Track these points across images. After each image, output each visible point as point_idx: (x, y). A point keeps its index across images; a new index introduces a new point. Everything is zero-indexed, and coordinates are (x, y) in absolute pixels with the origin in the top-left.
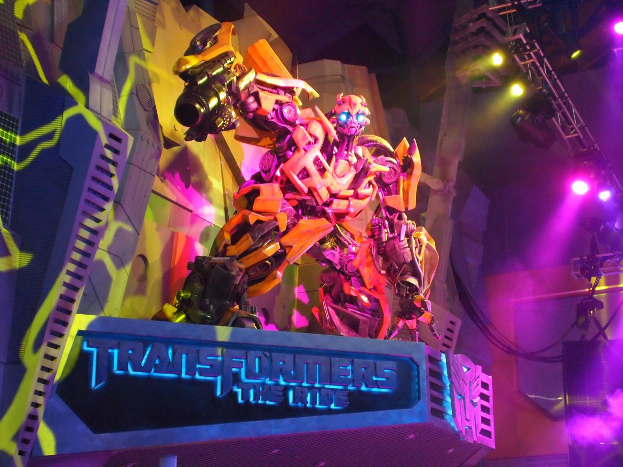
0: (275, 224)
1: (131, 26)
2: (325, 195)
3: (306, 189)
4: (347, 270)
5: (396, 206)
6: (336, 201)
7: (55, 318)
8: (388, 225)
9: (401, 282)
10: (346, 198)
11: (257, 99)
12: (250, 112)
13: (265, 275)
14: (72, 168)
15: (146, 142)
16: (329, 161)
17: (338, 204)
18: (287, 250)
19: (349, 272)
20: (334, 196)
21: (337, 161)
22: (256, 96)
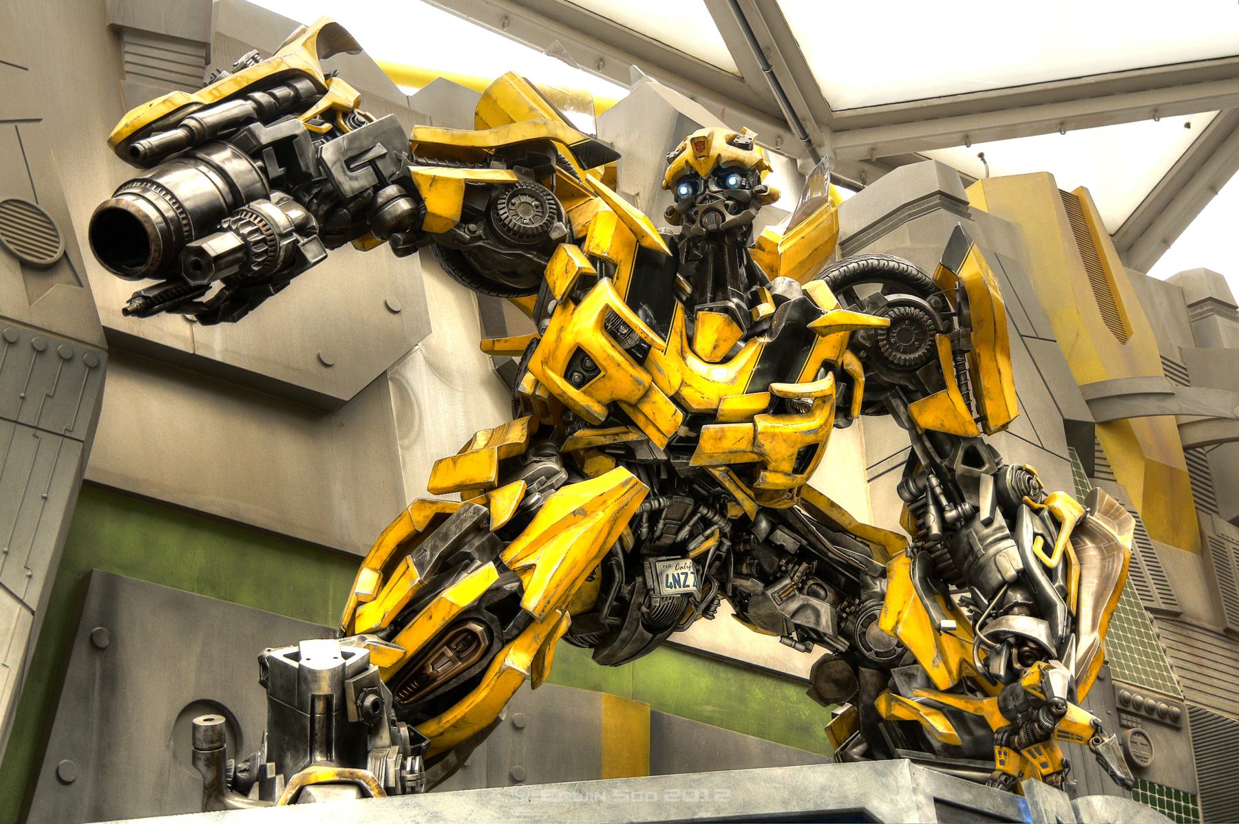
1: (1021, 336)
3: (598, 410)
4: (870, 650)
5: (952, 426)
11: (410, 189)
13: (476, 671)
14: (25, 567)
16: (661, 324)
17: (720, 438)
19: (877, 653)
20: (698, 419)
21: (691, 319)
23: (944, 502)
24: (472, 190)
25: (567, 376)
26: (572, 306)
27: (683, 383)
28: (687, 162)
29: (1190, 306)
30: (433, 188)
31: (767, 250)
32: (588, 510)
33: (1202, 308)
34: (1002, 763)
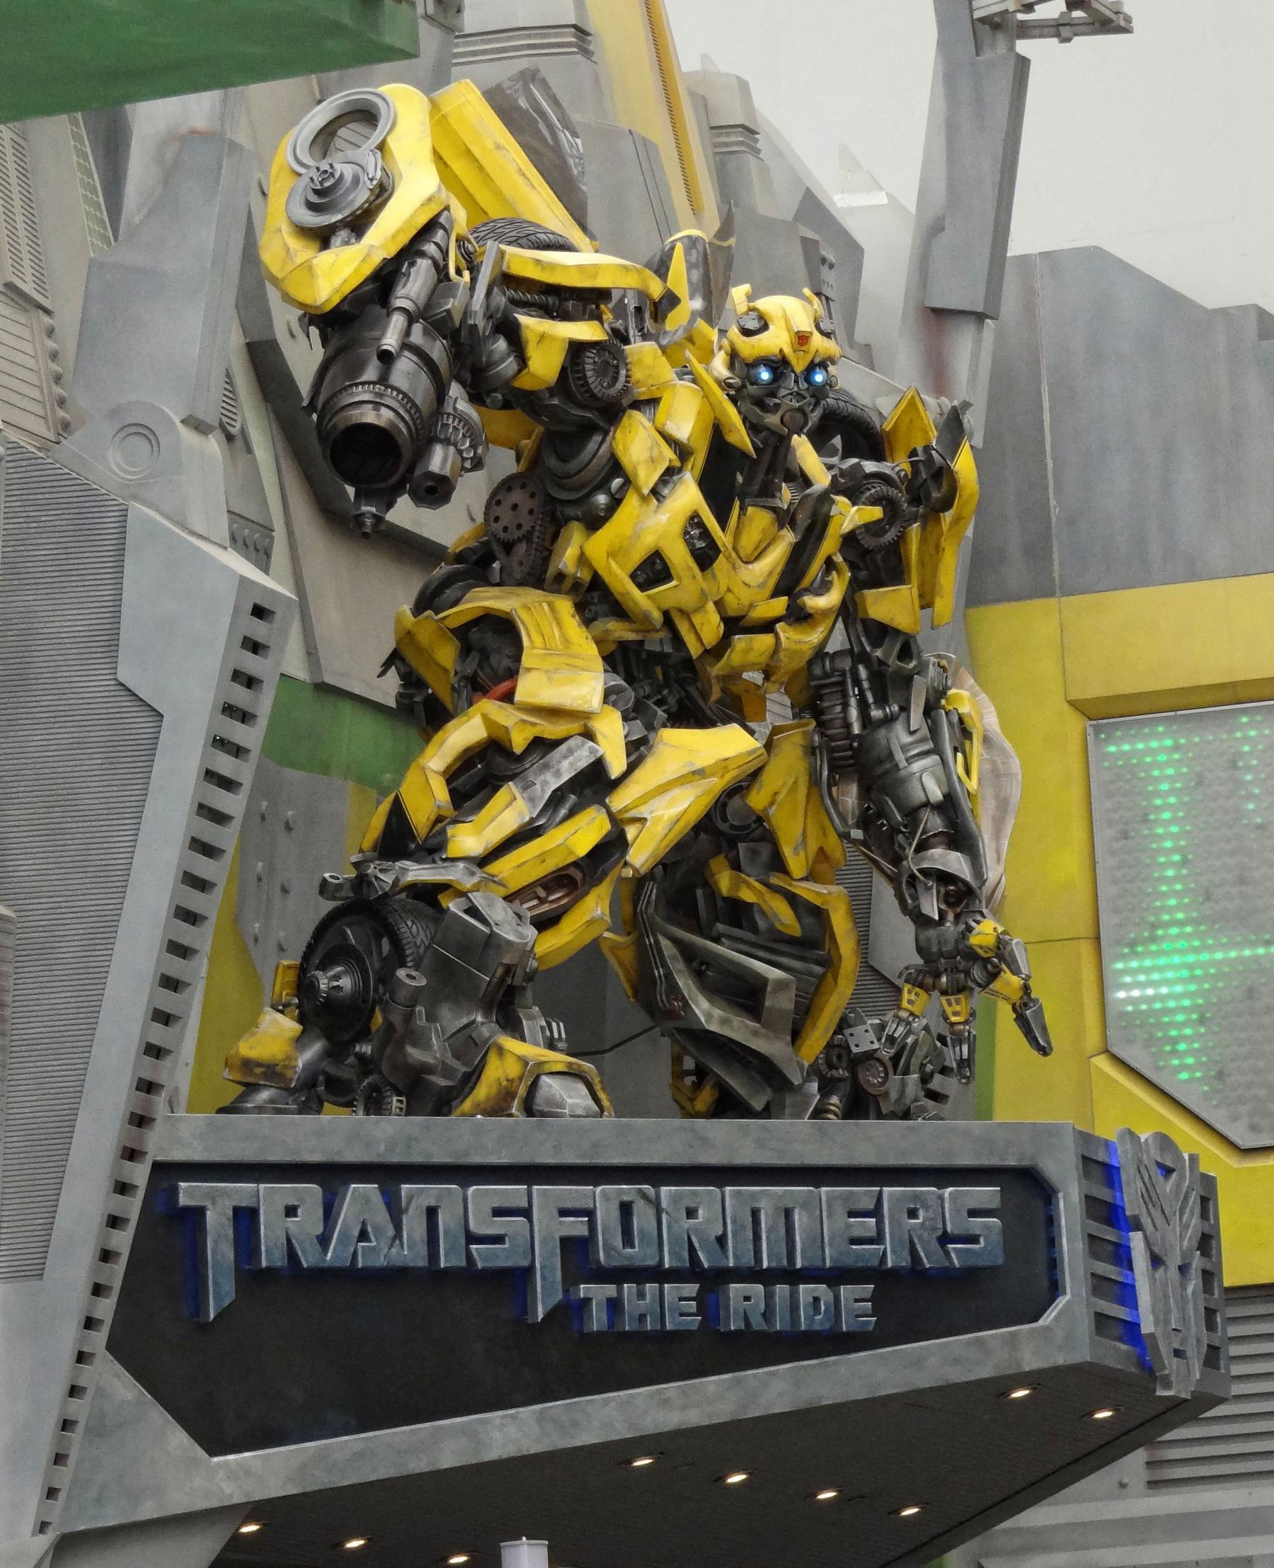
0: (592, 751)
2: (710, 626)
4: (725, 819)
6: (740, 641)
7: (125, 1148)
8: (869, 679)
9: (919, 870)
10: (767, 626)
12: (495, 390)
15: (242, 543)
18: (631, 832)
19: (732, 827)
20: (735, 625)
22: (512, 333)
23: (870, 698)
24: (576, 349)
25: (633, 576)
26: (655, 501)
27: (729, 590)
28: (781, 350)
29: (713, 128)
30: (540, 345)
31: (697, 345)
32: (708, 772)
33: (728, 134)
34: (910, 1002)
